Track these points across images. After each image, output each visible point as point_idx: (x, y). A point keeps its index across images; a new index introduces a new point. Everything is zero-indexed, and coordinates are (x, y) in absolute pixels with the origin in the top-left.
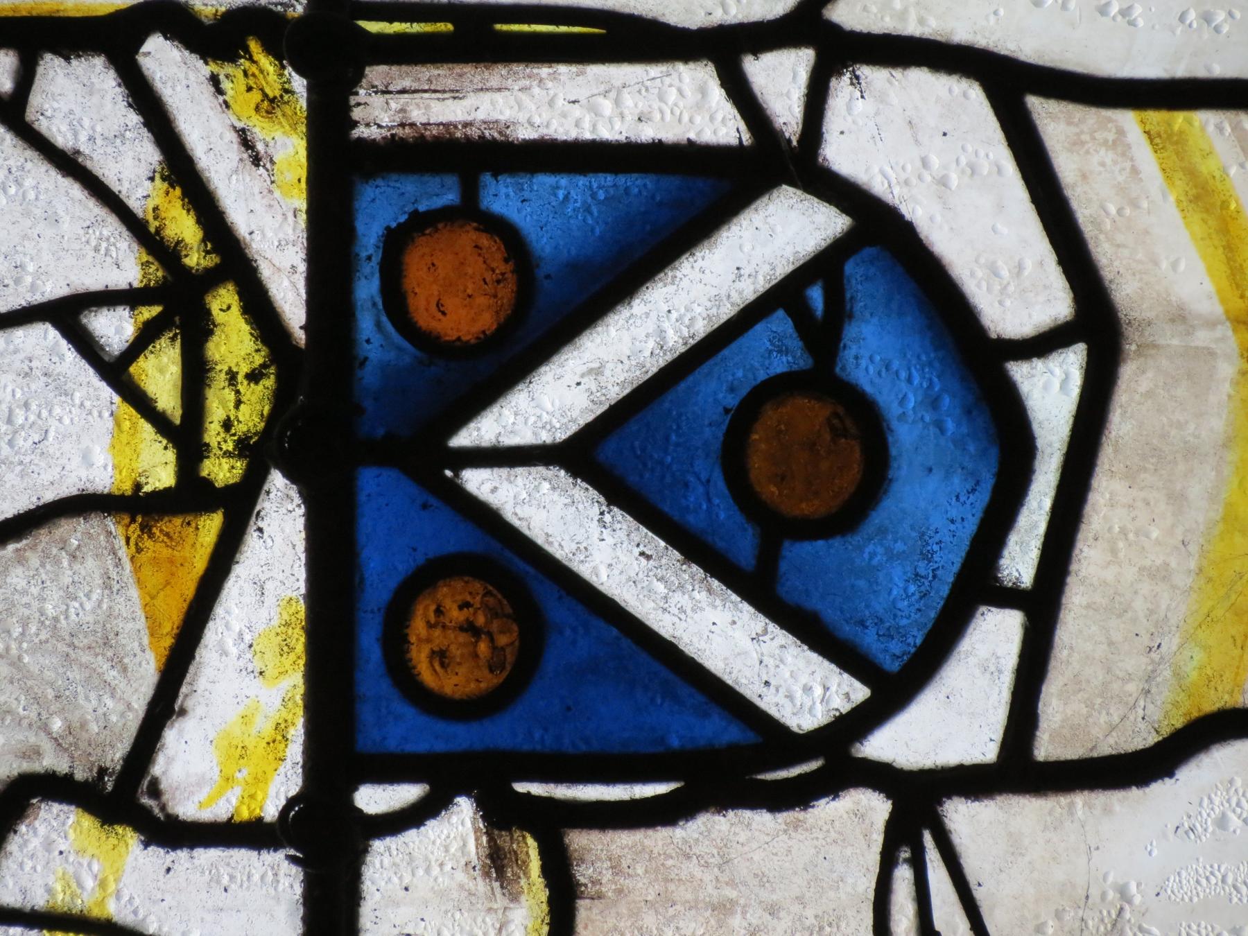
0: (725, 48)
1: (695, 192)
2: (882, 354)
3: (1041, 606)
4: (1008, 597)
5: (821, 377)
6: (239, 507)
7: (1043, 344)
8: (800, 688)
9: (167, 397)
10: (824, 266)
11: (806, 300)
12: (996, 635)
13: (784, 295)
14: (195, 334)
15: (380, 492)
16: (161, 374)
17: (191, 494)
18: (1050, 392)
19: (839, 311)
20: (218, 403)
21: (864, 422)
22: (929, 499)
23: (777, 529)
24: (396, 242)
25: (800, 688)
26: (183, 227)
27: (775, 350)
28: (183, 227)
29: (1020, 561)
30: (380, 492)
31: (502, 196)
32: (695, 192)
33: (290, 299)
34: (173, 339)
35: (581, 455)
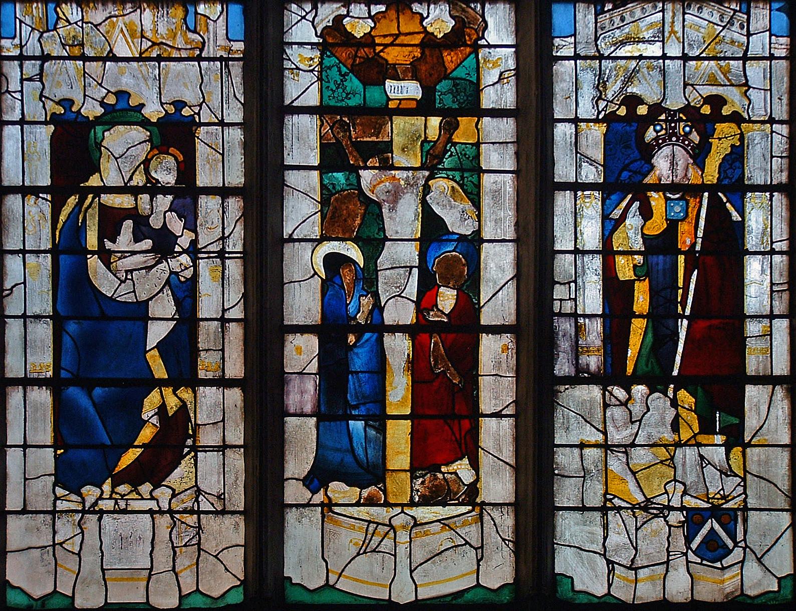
0: (745, 540)
1: (733, 537)
2: (721, 551)
3: (701, 564)
4: (702, 561)
5: (719, 547)
6: (708, 502)
7: (641, 316)
8: (694, 546)
9: (716, 497)
10: (727, 547)
11: (725, 546)
12: (699, 560)
13: (725, 544)
14: (721, 499)
15: (708, 513)
16: (718, 496)
17: (709, 498)
18: (718, 565)
19: (724, 548)
20: (716, 501)
21: (715, 550)
22: (710, 555)
23: (707, 543)
24: (729, 515)
25: (694, 546)
26: (730, 498)
27: (721, 544)
28: (730, 498)
29: (704, 562)
30: (708, 513)
31: (732, 522)
32: (733, 537)
33: (724, 506)
34: (242, 324)
35: (712, 528)
